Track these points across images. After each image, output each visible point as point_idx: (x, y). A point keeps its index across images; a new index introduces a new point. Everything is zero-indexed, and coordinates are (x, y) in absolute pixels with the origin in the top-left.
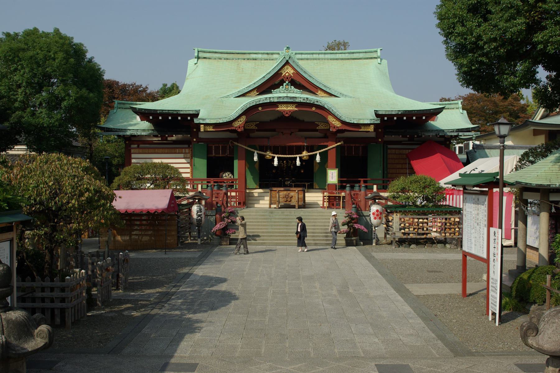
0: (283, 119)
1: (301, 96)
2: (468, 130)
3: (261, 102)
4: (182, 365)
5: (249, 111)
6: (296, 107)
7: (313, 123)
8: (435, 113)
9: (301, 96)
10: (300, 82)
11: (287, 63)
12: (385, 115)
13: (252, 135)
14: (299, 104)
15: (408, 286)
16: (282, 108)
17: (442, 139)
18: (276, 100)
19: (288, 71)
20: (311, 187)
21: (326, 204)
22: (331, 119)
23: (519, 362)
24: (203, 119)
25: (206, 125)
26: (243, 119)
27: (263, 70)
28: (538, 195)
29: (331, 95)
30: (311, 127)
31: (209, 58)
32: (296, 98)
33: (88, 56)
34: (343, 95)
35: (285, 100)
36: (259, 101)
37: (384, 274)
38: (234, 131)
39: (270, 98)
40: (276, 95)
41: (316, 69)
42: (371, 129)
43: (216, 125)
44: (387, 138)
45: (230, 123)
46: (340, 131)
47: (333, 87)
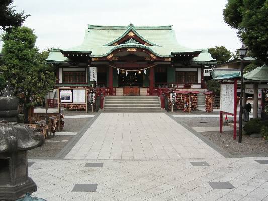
0: (131, 55)
1: (138, 45)
2: (212, 61)
4: (91, 164)
5: (114, 52)
7: (143, 57)
8: (196, 54)
9: (138, 45)
10: (137, 39)
12: (175, 54)
13: (115, 63)
14: (139, 49)
15: (193, 128)
16: (129, 50)
17: (199, 66)
20: (141, 86)
21: (149, 94)
22: (152, 55)
23: (33, 165)
24: (94, 55)
26: (111, 55)
27: (119, 35)
28: (252, 86)
30: (142, 59)
33: (226, 8)
35: (131, 46)
37: (180, 123)
38: (108, 61)
41: (142, 34)
42: (170, 60)
44: (176, 65)
45: (106, 57)
46: (155, 61)
47: (152, 42)
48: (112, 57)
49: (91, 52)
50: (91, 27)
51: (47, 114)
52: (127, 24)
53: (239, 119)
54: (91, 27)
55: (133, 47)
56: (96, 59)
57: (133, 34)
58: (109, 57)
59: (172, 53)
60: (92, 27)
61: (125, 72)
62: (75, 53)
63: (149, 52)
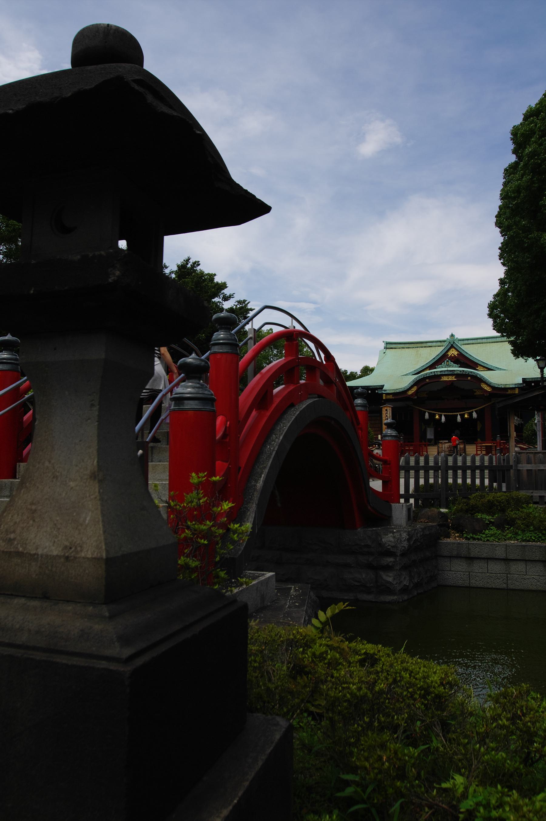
5: (416, 383)
6: (455, 378)
10: (463, 360)
16: (445, 379)
18: (439, 373)
19: (453, 352)
25: (387, 394)
26: (415, 389)
27: (435, 353)
29: (489, 369)
31: (395, 348)
34: (498, 368)
35: (446, 373)
38: (409, 398)
39: (434, 372)
40: (439, 369)
41: (474, 352)
42: (517, 392)
43: (394, 394)
45: (405, 392)
47: (490, 362)
48: (417, 392)
49: (383, 386)
50: (388, 346)
51: (277, 451)
52: (445, 336)
53: (531, 361)
54: (388, 346)
55: (452, 373)
56: (389, 397)
57: (456, 353)
58: (410, 393)
59: (524, 380)
60: (389, 346)
61: (440, 416)
62: (354, 379)
63: (481, 380)
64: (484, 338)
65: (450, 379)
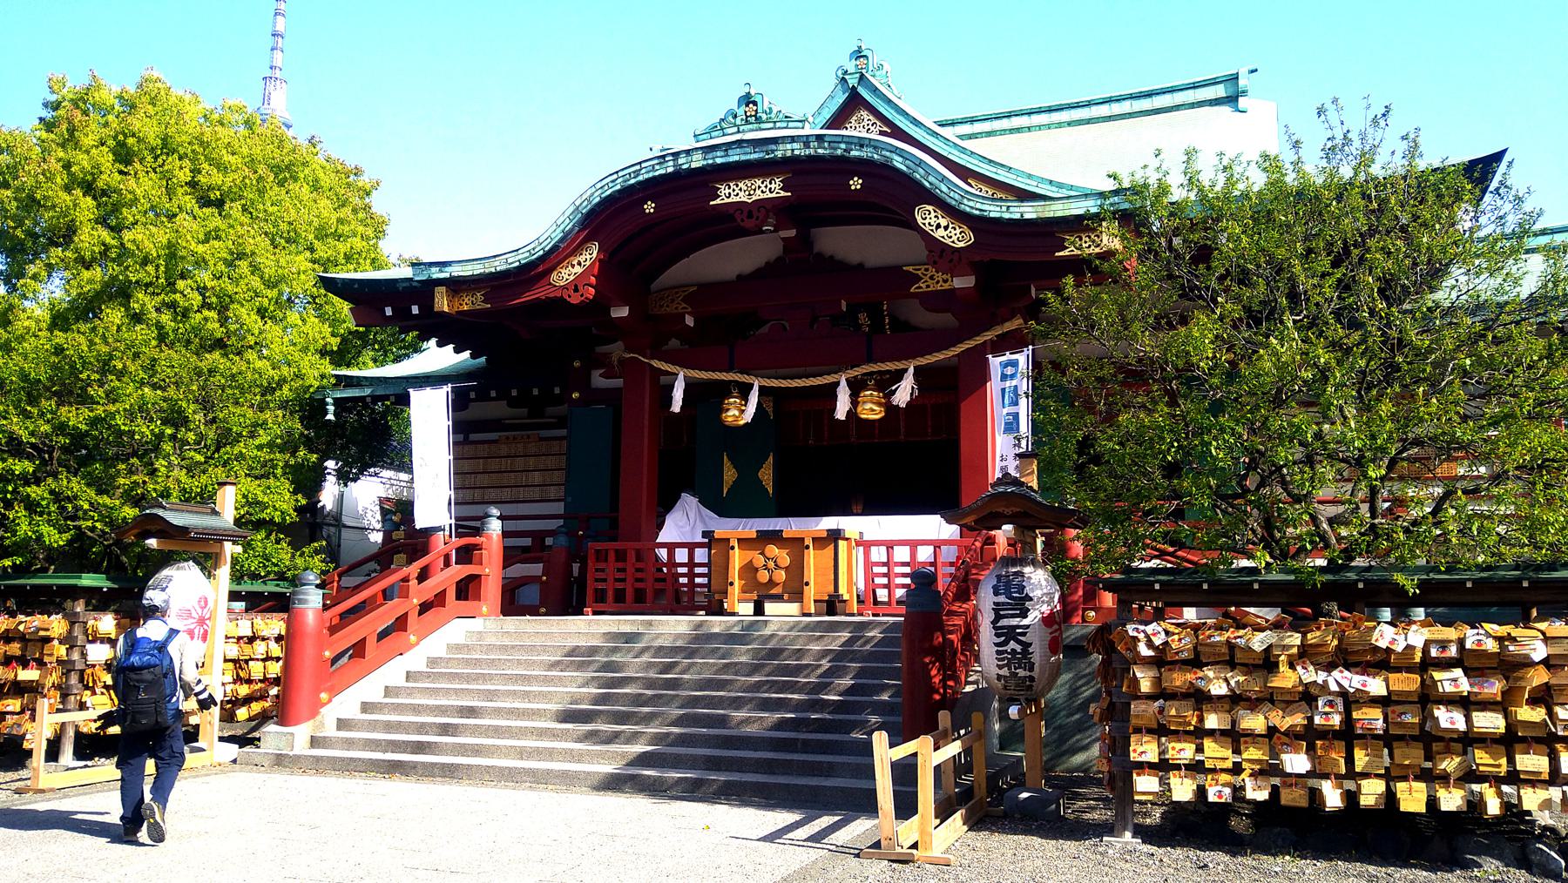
3: (640, 178)
11: (854, 103)
32: (775, 141)
35: (734, 156)
36: (637, 173)
64: (1039, 111)
65: (758, 195)
